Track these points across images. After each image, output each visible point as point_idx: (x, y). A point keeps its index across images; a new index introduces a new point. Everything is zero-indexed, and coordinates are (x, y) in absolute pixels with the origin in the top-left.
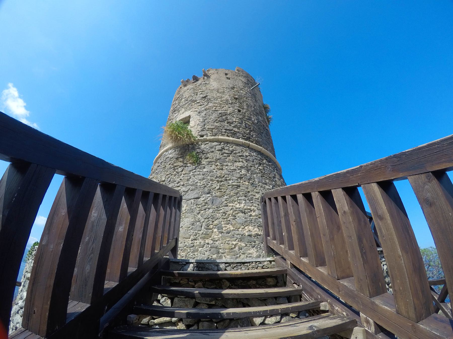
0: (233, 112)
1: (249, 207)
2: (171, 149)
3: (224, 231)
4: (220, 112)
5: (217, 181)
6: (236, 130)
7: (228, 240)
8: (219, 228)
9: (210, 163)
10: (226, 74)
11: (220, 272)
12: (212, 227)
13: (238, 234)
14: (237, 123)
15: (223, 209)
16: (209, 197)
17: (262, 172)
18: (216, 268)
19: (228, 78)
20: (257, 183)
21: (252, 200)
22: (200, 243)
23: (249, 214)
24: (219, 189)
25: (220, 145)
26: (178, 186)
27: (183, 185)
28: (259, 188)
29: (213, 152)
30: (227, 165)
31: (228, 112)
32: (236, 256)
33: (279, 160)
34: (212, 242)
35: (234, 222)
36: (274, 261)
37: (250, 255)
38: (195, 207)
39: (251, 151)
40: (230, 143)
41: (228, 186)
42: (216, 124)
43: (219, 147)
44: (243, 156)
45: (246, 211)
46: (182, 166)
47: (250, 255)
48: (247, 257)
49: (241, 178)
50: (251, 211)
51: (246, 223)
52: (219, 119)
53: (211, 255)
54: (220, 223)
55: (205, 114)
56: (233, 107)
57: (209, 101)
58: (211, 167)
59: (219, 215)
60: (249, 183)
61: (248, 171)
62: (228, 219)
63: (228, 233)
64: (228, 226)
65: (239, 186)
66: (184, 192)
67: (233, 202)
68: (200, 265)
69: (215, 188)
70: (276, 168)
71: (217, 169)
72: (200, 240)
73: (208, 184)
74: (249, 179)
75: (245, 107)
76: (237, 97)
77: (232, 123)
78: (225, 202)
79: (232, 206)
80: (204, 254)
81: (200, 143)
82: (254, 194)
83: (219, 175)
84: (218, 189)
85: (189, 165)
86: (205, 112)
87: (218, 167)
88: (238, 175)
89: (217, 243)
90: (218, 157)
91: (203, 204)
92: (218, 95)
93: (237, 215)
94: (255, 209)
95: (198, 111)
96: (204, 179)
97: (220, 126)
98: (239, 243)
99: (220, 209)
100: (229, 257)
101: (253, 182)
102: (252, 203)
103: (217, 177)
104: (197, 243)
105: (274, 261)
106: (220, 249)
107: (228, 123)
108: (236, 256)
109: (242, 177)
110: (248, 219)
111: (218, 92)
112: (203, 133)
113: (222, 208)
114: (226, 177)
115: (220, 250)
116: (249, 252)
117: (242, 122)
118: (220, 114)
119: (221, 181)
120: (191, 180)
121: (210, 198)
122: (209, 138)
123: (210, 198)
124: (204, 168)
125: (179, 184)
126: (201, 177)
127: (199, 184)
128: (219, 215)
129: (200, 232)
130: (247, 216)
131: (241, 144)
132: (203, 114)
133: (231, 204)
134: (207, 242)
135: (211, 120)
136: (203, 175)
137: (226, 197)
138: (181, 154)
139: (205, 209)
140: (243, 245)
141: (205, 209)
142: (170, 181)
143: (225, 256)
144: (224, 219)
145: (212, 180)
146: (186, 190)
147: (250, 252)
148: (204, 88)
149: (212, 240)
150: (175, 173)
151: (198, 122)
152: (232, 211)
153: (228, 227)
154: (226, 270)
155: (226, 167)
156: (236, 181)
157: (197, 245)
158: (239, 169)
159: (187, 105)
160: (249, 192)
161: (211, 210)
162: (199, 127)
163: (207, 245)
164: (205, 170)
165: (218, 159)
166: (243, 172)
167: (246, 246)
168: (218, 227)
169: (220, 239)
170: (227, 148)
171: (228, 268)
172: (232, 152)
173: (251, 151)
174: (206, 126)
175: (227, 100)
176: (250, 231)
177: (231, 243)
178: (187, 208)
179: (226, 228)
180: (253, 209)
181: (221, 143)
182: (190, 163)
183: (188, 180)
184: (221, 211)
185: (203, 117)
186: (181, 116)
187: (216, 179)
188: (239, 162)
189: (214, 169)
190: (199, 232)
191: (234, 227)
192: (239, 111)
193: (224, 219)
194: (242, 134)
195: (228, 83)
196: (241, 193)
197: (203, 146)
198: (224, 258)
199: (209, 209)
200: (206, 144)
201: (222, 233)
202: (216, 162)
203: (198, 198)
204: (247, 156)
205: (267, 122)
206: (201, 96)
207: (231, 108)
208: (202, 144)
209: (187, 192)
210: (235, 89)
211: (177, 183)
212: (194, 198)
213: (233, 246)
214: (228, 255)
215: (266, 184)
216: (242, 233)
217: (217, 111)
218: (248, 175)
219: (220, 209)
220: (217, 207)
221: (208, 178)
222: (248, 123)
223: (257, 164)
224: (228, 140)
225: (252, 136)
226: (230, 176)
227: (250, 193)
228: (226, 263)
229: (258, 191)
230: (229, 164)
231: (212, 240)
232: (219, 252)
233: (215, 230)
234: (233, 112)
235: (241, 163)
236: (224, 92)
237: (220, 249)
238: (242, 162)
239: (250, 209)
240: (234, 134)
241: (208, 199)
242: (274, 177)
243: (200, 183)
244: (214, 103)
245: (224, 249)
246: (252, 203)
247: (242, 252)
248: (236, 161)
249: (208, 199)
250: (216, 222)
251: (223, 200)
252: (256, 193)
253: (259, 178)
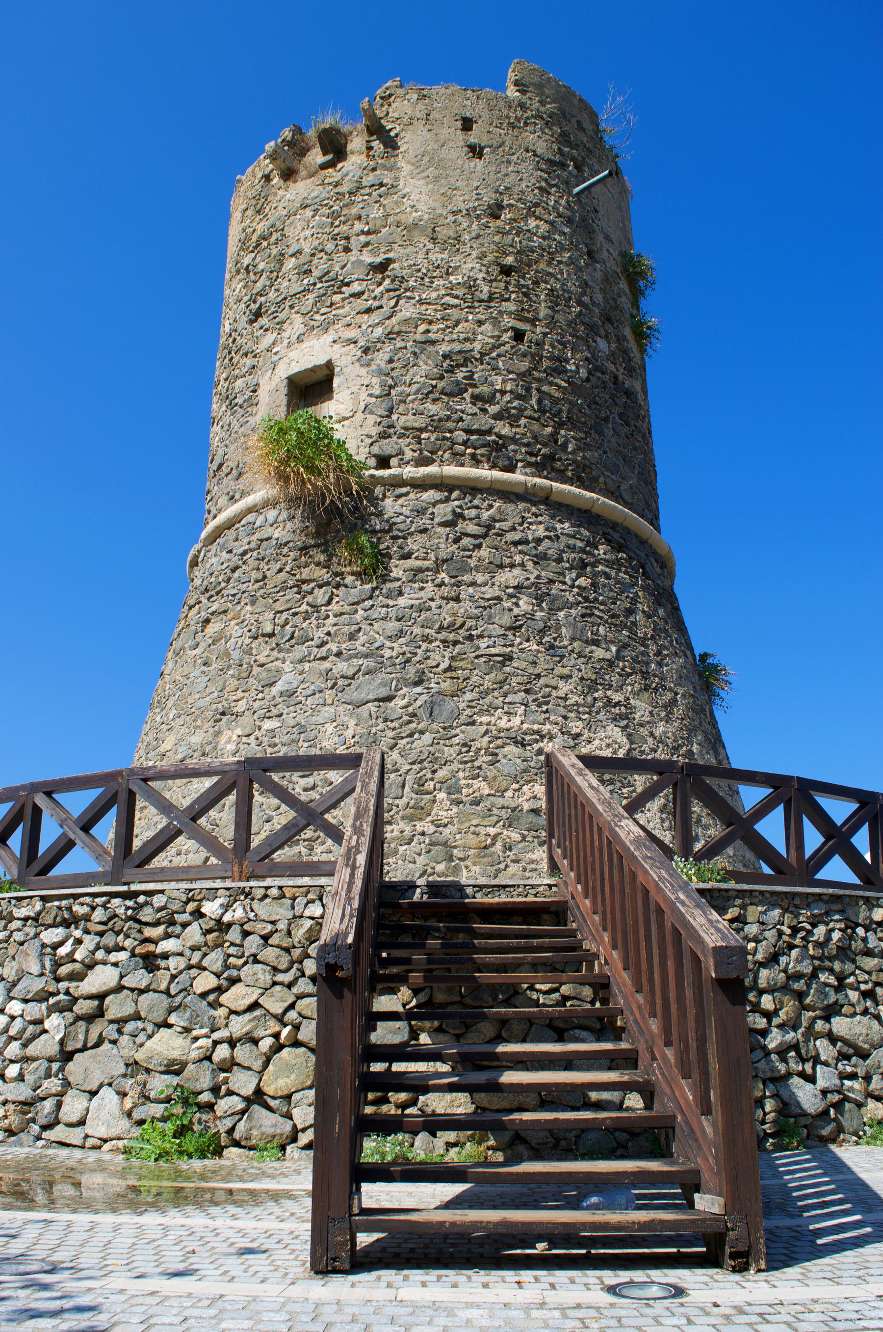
0: (494, 347)
1: (536, 727)
2: (268, 504)
3: (464, 799)
4: (444, 348)
5: (444, 641)
6: (504, 429)
7: (474, 822)
8: (453, 790)
9: (420, 576)
10: (467, 124)
11: (467, 900)
12: (432, 787)
13: (503, 807)
14: (507, 397)
15: (463, 732)
16: (420, 694)
17: (586, 599)
18: (459, 894)
19: (476, 151)
20: (566, 643)
21: (547, 703)
22: (402, 832)
23: (536, 746)
24: (450, 669)
25: (447, 500)
26: (324, 659)
27: (339, 654)
28: (573, 662)
29: (424, 531)
30: (473, 584)
31: (477, 346)
32: (496, 867)
33: (673, 535)
34: (432, 829)
35: (491, 772)
36: (555, 885)
37: (533, 866)
38: (381, 726)
39: (553, 517)
40: (481, 491)
41: (477, 657)
42: (433, 408)
43: (443, 511)
44: (526, 542)
45: (528, 738)
46: (328, 584)
47: (533, 866)
48: (525, 869)
49: (515, 629)
50: (542, 737)
51: (520, 778)
52: (441, 384)
53: (432, 865)
54: (454, 774)
55: (391, 361)
56: (495, 322)
57: (399, 290)
58: (422, 589)
59: (450, 752)
60: (540, 643)
61: (539, 599)
62: (476, 764)
63: (476, 803)
64: (476, 784)
65: (511, 659)
66: (343, 677)
67: (491, 709)
68: (434, 888)
69: (437, 666)
70: (651, 568)
71: (443, 598)
72: (402, 825)
73: (415, 654)
74: (542, 632)
75: (543, 312)
76: (510, 260)
77: (491, 400)
78: (468, 712)
79: (488, 724)
80: (415, 862)
81: (378, 490)
82: (553, 682)
83: (449, 619)
84: (446, 671)
85: (349, 579)
86: (388, 348)
87: (445, 591)
88: (507, 620)
89: (446, 831)
90: (443, 555)
91: (406, 718)
92: (436, 256)
93: (501, 752)
94: (555, 730)
95: (362, 343)
96: (401, 634)
97: (448, 418)
98: (505, 832)
99: (454, 732)
100: (476, 869)
101: (555, 639)
102: (547, 711)
103: (441, 628)
104: (392, 831)
105: (555, 885)
106: (455, 847)
107: (476, 398)
108: (496, 867)
109: (521, 626)
110: (532, 764)
111: (434, 240)
112: (387, 447)
113: (458, 731)
114: (470, 629)
115: (455, 851)
116: (530, 856)
117: (528, 389)
118: (445, 357)
119: (456, 643)
120: (362, 638)
121: (424, 698)
122: (410, 472)
123: (424, 698)
124: (401, 594)
125: (323, 651)
126: (392, 626)
127: (387, 653)
128: (450, 752)
129: (402, 802)
130: (528, 754)
131: (521, 490)
132: (380, 358)
133: (485, 719)
134: (419, 828)
135: (414, 387)
136: (399, 620)
137: (468, 696)
138: (317, 535)
139: (411, 735)
140: (515, 836)
141: (411, 735)
142: (292, 637)
143: (467, 867)
144: (466, 763)
145: (426, 639)
146: (350, 672)
147: (534, 857)
148: (376, 213)
149: (432, 822)
150: (304, 607)
151: (363, 396)
152: (486, 739)
153: (475, 787)
154: (474, 897)
155: (471, 590)
156: (500, 641)
157: (393, 839)
158: (510, 596)
159: (311, 297)
160: (538, 676)
161: (427, 738)
162: (372, 419)
163: (422, 838)
164: (402, 602)
165: (445, 561)
166: (525, 604)
167: (524, 838)
168: (449, 788)
169: (456, 820)
170: (473, 513)
171: (478, 895)
172: (489, 527)
173: (553, 517)
174: (394, 417)
175: (471, 286)
176: (535, 797)
177: (482, 831)
178: (359, 730)
179: (471, 791)
180: (549, 733)
181: (451, 492)
182: (353, 574)
183: (352, 637)
184: (456, 740)
185: (380, 372)
186: (293, 354)
187: (440, 636)
188: (512, 566)
189: (432, 600)
190: (397, 802)
191: (491, 787)
192: (519, 336)
193: (466, 763)
194: (528, 445)
195: (474, 182)
196: (514, 681)
197: (390, 506)
198: (464, 871)
199: (422, 732)
200: (399, 497)
201: (459, 803)
202: (438, 572)
203: (389, 699)
204: (538, 541)
205: (632, 344)
206: (368, 258)
207: (487, 327)
208: (384, 496)
209: (353, 678)
210: (506, 215)
211: (318, 647)
212: (375, 700)
213: (489, 841)
214: (475, 864)
215: (596, 643)
216: (513, 805)
217: (433, 343)
218: (539, 615)
219: (454, 732)
220: (444, 728)
221: (417, 630)
222: (553, 390)
223: (570, 569)
224: (477, 479)
225: (565, 445)
226: (481, 623)
227: (542, 681)
228: (474, 886)
229: (566, 671)
230: (480, 578)
231: (432, 822)
232: (452, 856)
233: (442, 795)
234: (494, 347)
235: (517, 571)
236: (458, 239)
237: (455, 847)
238: (522, 565)
239: (538, 732)
240: (497, 452)
241: (419, 703)
242: (630, 612)
243: (392, 648)
244: (421, 302)
245: (465, 848)
246: (547, 711)
247: (513, 857)
248: (501, 566)
249: (419, 703)
250: (442, 774)
251: (462, 705)
252: (562, 677)
253: (575, 626)
